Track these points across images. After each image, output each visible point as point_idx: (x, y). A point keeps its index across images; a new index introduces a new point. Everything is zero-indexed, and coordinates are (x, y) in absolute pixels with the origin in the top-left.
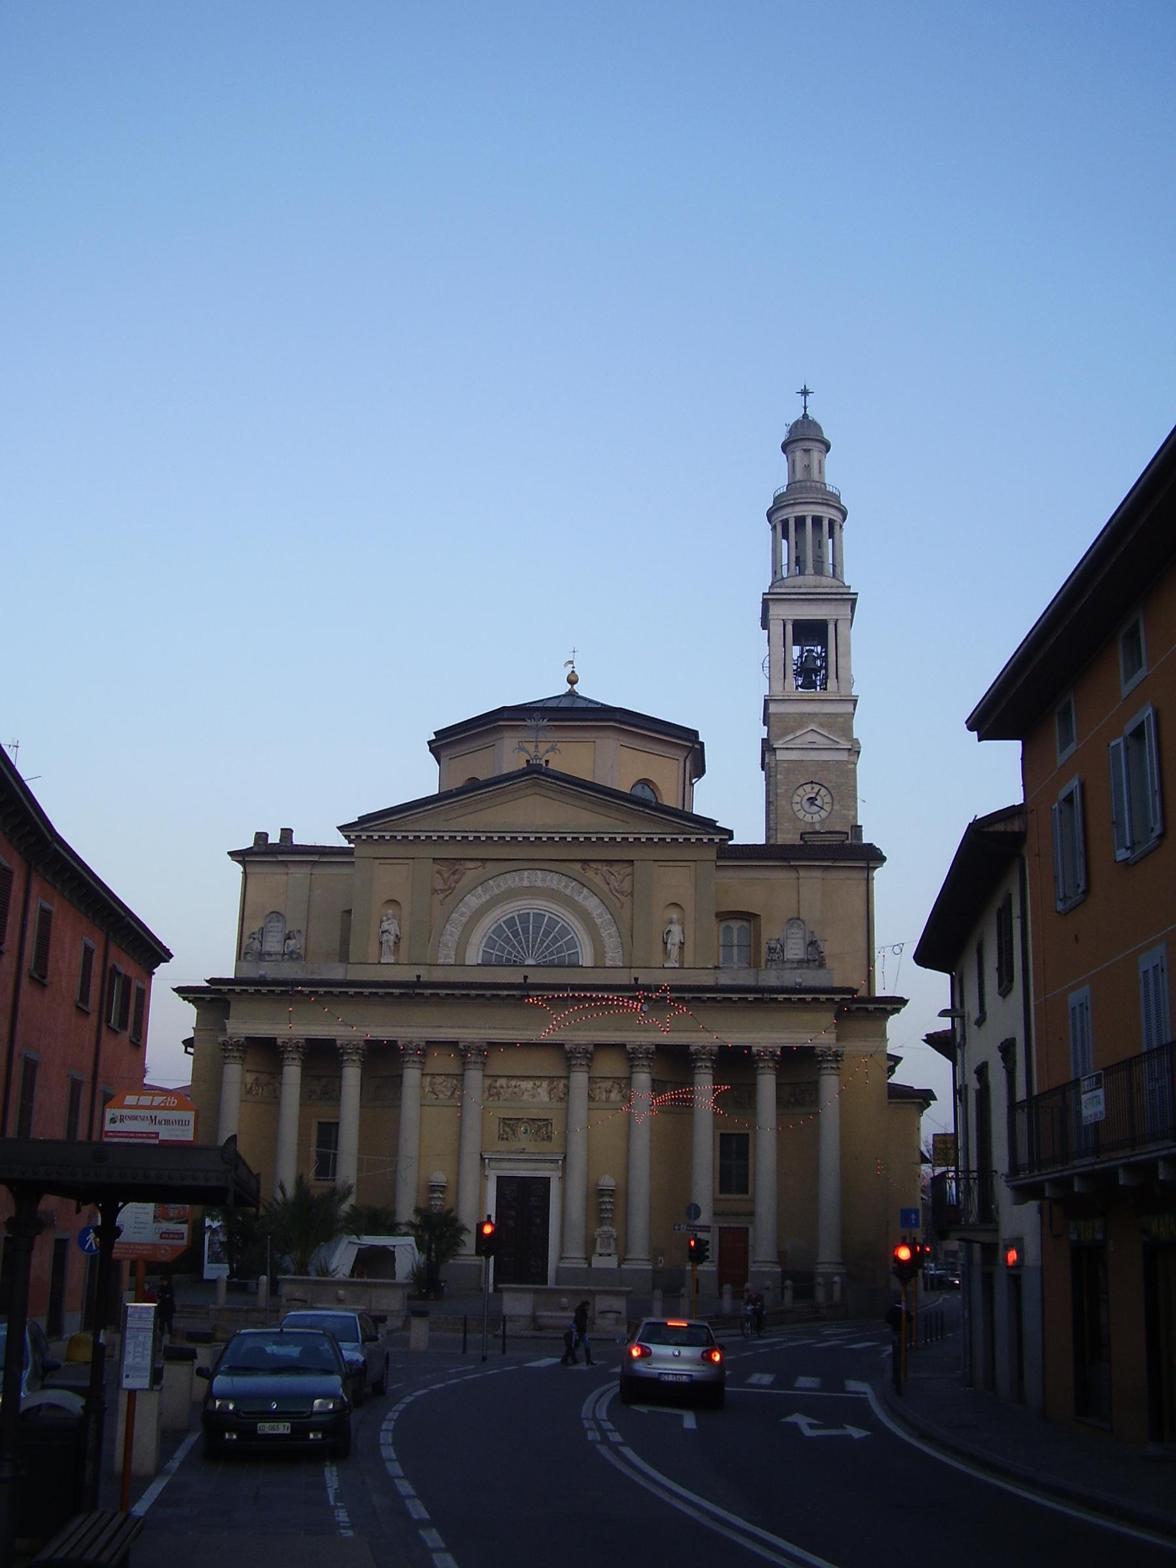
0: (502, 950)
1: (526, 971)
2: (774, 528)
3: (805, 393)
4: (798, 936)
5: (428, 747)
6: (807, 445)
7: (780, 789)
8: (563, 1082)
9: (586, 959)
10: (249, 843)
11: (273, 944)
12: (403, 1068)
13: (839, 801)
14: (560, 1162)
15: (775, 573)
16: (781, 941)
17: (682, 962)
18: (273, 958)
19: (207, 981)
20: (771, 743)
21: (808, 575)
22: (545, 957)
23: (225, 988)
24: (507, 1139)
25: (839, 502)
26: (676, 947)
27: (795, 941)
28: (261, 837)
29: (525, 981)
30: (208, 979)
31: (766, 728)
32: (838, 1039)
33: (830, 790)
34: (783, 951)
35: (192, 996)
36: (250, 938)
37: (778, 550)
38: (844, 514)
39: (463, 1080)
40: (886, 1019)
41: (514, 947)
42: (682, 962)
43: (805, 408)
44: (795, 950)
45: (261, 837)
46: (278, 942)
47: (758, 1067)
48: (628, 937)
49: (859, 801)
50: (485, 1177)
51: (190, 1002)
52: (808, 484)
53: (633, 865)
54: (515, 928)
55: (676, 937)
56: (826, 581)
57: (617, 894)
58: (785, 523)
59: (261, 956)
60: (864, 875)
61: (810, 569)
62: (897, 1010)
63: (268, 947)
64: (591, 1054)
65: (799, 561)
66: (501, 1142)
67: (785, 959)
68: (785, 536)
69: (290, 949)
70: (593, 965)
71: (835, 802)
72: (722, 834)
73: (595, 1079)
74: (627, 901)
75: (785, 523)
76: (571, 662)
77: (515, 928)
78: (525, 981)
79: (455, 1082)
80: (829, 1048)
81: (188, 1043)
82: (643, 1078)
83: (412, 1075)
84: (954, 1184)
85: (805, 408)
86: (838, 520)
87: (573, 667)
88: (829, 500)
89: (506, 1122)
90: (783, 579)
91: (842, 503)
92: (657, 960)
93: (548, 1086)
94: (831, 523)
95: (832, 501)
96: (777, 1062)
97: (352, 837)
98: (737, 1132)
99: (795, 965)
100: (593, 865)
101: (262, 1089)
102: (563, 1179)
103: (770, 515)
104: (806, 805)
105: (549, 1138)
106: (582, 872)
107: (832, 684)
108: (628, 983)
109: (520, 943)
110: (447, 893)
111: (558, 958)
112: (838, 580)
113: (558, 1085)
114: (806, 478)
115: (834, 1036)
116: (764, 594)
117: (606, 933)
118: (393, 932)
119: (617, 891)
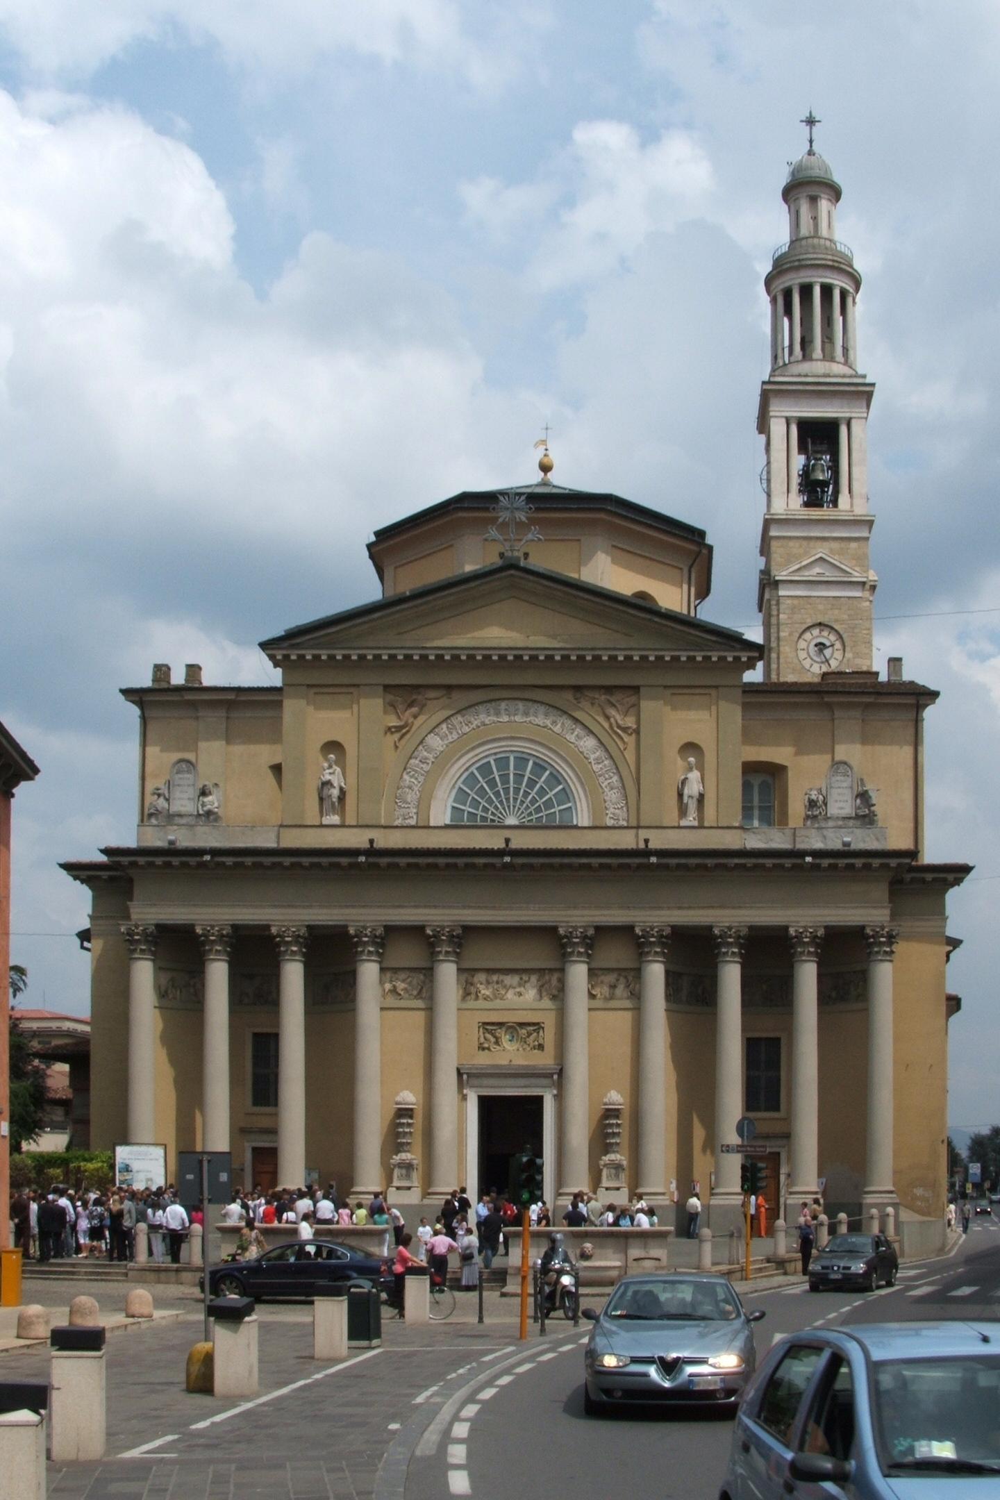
0: (475, 804)
1: (508, 834)
2: (774, 301)
3: (811, 122)
4: (845, 785)
5: (367, 553)
6: (813, 191)
7: (783, 631)
8: (556, 976)
9: (583, 817)
10: (145, 680)
11: (184, 802)
12: (356, 962)
13: (852, 648)
14: (555, 1077)
15: (775, 358)
16: (824, 792)
17: (701, 816)
18: (184, 821)
19: (102, 851)
20: (773, 574)
21: (817, 360)
22: (530, 814)
23: (125, 860)
24: (489, 1049)
25: (851, 266)
26: (695, 800)
27: (839, 790)
28: (161, 671)
29: (507, 845)
30: (103, 847)
31: (763, 559)
32: (894, 916)
33: (841, 633)
34: (825, 804)
35: (84, 874)
36: (154, 794)
37: (779, 328)
38: (857, 283)
39: (432, 975)
40: (946, 891)
41: (490, 801)
42: (701, 816)
43: (811, 141)
44: (841, 804)
45: (161, 671)
46: (189, 799)
47: (796, 952)
48: (634, 786)
49: (874, 649)
50: (464, 1098)
51: (83, 881)
52: (816, 241)
53: (639, 692)
54: (491, 777)
55: (693, 788)
56: (837, 368)
57: (618, 731)
58: (788, 294)
59: (171, 818)
60: (912, 715)
61: (818, 352)
62: (958, 882)
63: (176, 807)
64: (590, 939)
65: (806, 343)
66: (481, 1052)
67: (829, 815)
68: (788, 311)
69: (205, 809)
70: (591, 825)
71: (848, 649)
72: (750, 650)
73: (596, 972)
74: (630, 740)
75: (788, 294)
76: (544, 442)
77: (491, 777)
78: (507, 845)
79: (422, 977)
80: (883, 928)
81: (84, 936)
82: (656, 972)
83: (369, 972)
84: (32, 1251)
85: (811, 141)
86: (851, 290)
87: (546, 450)
88: (840, 263)
89: (488, 1027)
90: (785, 365)
91: (855, 266)
92: (671, 817)
93: (538, 981)
94: (844, 294)
95: (844, 264)
96: (817, 946)
97: (279, 657)
98: (764, 1035)
99: (840, 823)
100: (589, 694)
101: (181, 992)
102: (560, 1098)
103: (769, 281)
104: (812, 649)
105: (541, 1047)
106: (575, 702)
107: (843, 500)
108: (634, 847)
109: (497, 794)
110: (404, 731)
111: (546, 815)
112: (851, 367)
113: (550, 980)
114: (812, 234)
115: (887, 912)
116: (764, 383)
117: (606, 783)
118: (336, 784)
119: (619, 727)
